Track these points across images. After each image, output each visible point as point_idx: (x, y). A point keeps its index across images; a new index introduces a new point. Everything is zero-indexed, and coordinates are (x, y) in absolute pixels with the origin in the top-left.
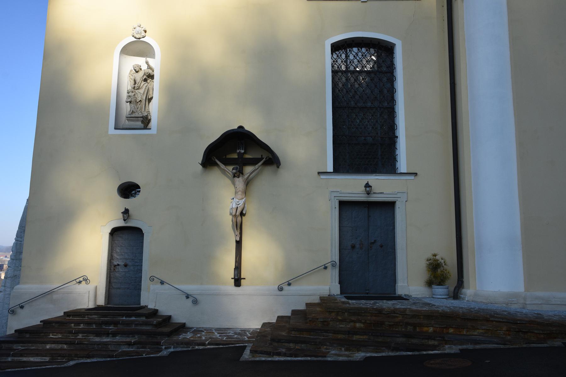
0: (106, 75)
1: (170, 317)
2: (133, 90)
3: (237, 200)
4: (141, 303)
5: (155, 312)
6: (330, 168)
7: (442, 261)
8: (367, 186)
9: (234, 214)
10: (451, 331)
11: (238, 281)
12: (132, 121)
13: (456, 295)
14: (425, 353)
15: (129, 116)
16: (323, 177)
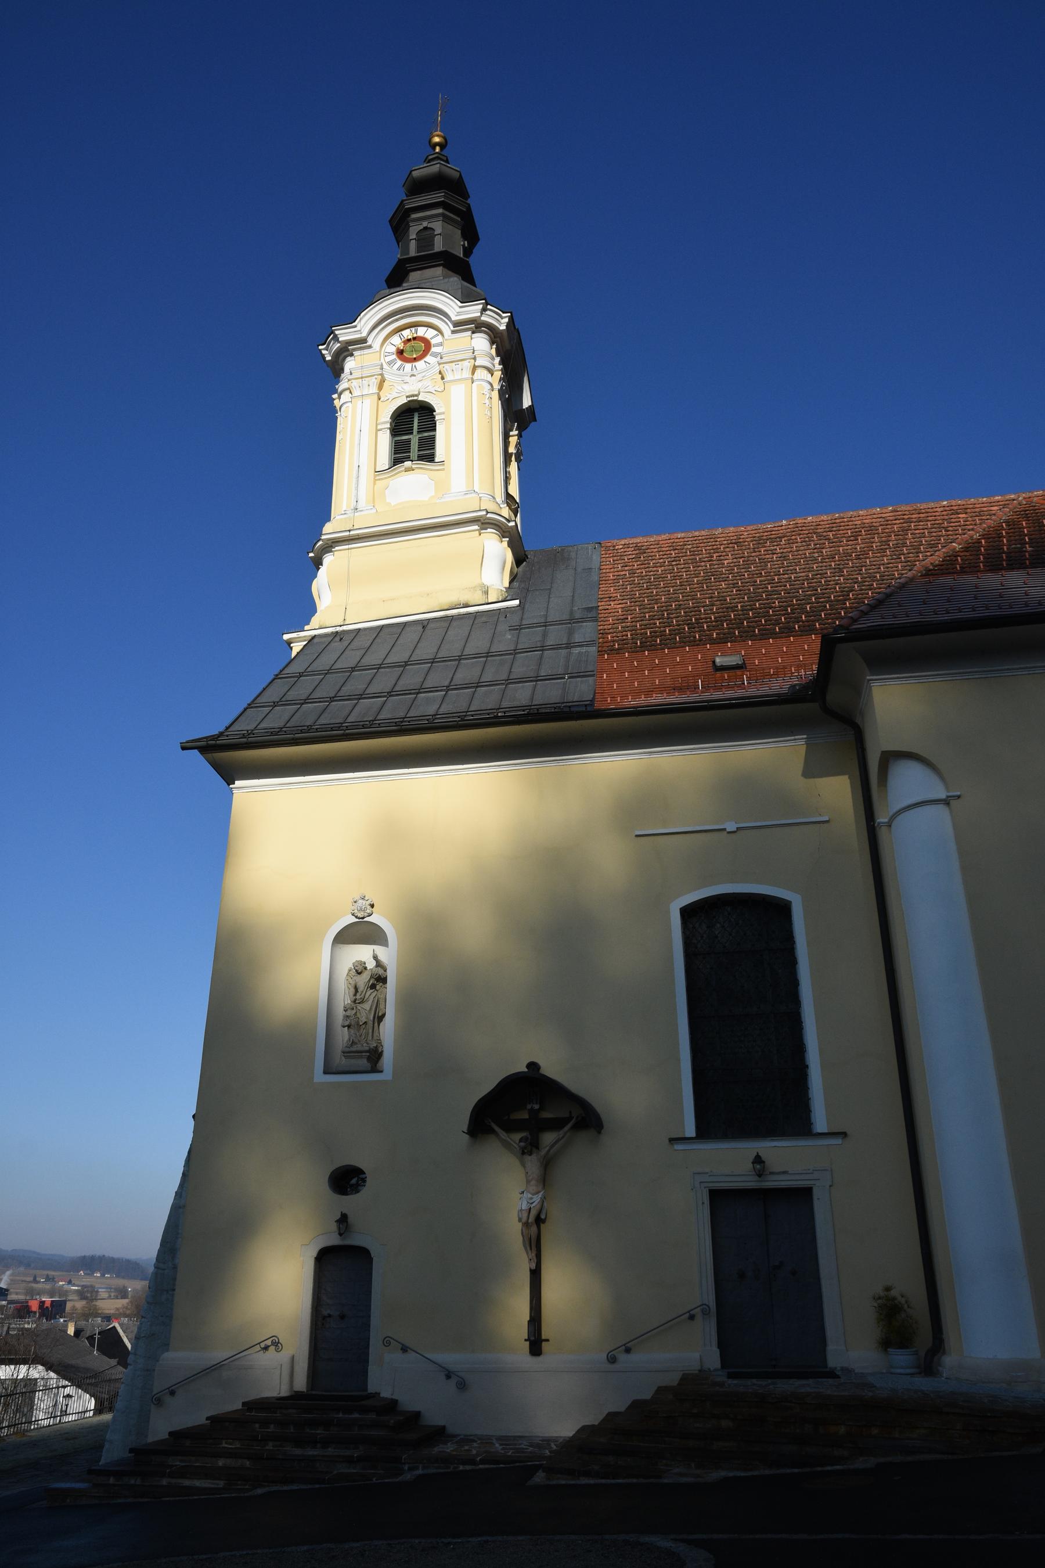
0: (310, 977)
1: (417, 1415)
2: (353, 1005)
3: (530, 1196)
4: (848, 781)
5: (392, 1405)
6: (690, 1131)
7: (903, 1301)
8: (758, 1160)
9: (524, 1219)
10: (875, 1431)
11: (536, 1345)
12: (354, 1057)
13: (928, 1366)
14: (819, 1469)
15: (347, 1050)
16: (679, 1147)
